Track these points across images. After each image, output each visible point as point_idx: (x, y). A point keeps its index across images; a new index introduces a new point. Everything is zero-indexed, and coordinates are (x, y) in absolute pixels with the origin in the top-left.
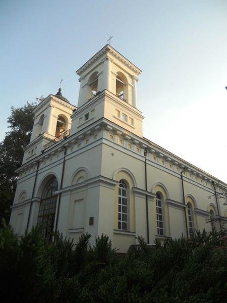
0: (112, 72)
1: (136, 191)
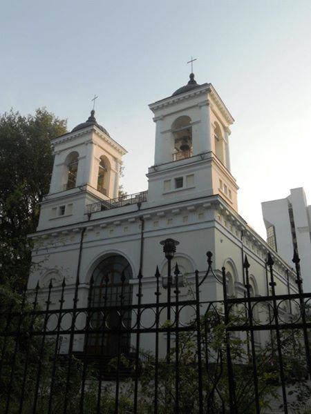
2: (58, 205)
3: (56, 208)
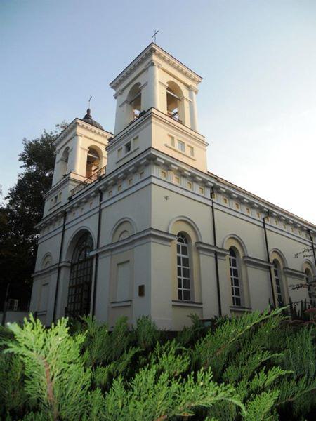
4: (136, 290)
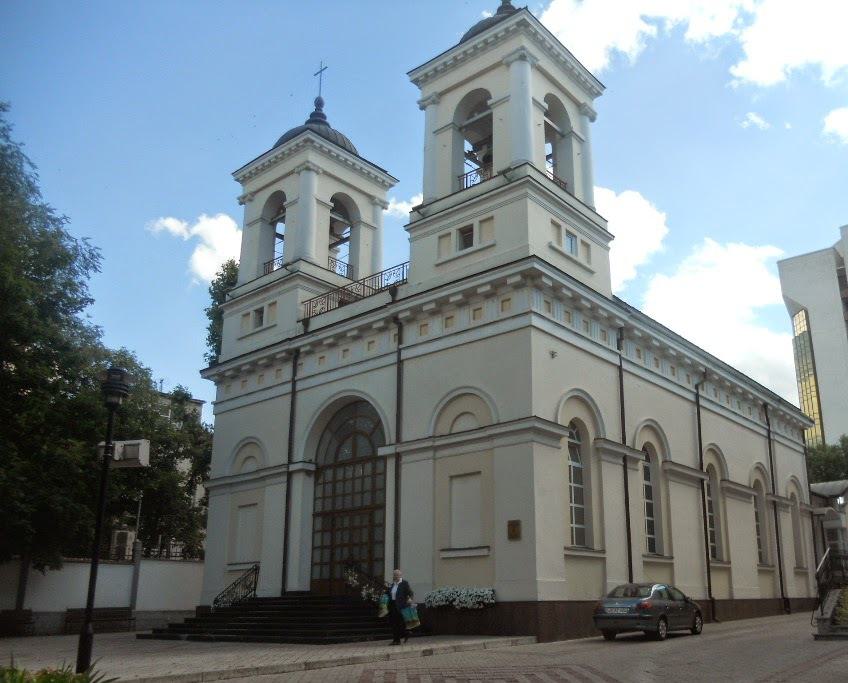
0: (533, 99)
1: (604, 450)
2: (251, 306)
3: (248, 314)
4: (502, 531)
